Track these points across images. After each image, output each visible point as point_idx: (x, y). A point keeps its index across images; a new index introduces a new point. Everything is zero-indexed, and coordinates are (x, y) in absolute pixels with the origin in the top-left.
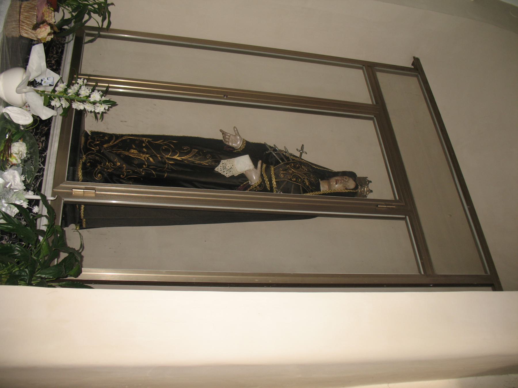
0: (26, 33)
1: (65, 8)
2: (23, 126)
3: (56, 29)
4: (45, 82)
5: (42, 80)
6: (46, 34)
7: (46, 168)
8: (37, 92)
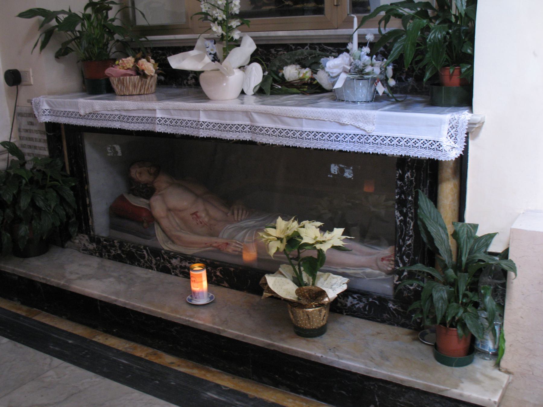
0: (151, 86)
1: (110, 51)
2: (264, 72)
3: (139, 56)
4: (212, 50)
5: (210, 54)
6: (149, 64)
7: (308, 42)
8: (225, 57)
